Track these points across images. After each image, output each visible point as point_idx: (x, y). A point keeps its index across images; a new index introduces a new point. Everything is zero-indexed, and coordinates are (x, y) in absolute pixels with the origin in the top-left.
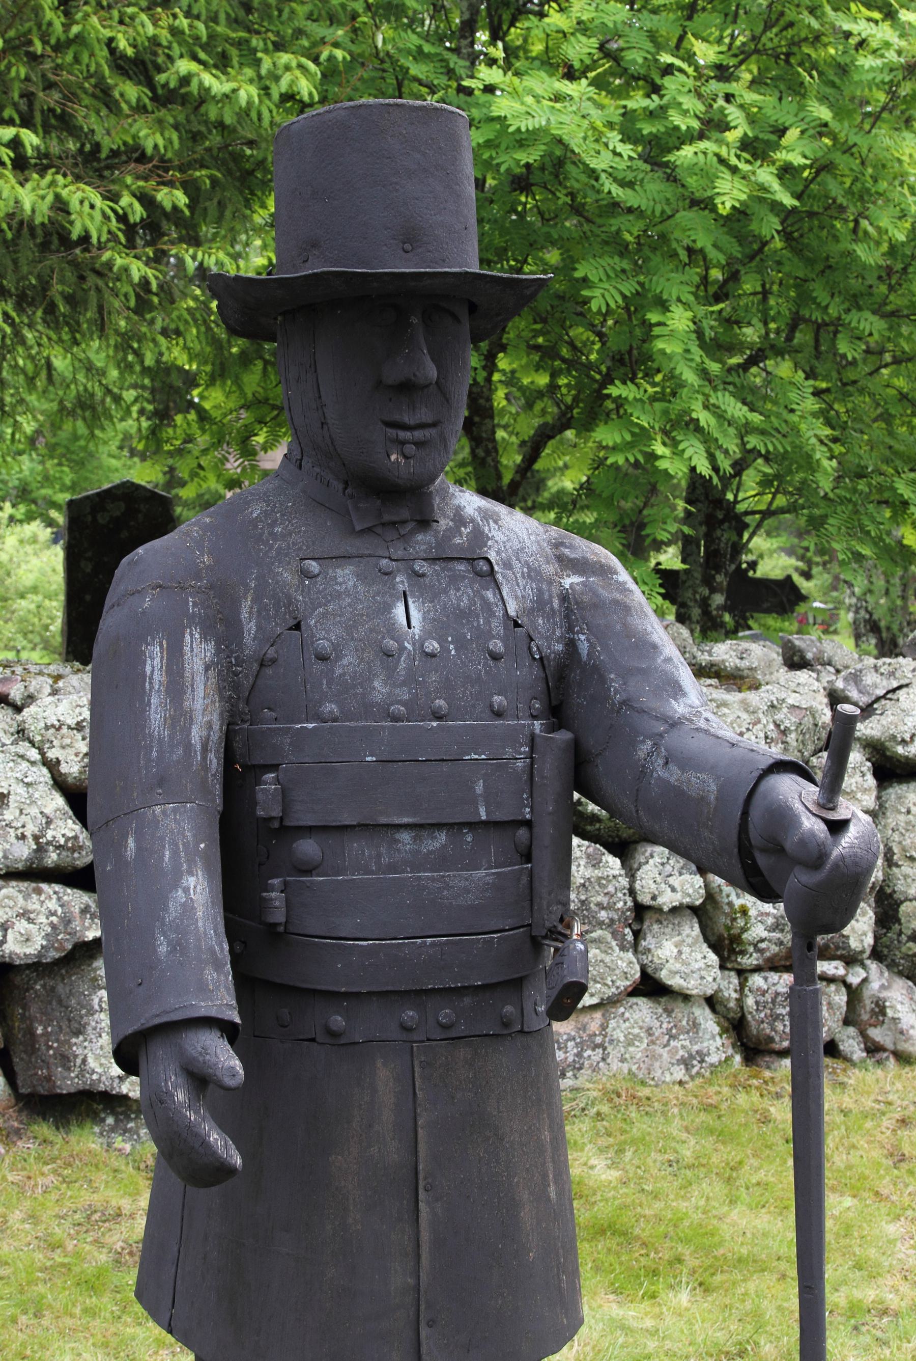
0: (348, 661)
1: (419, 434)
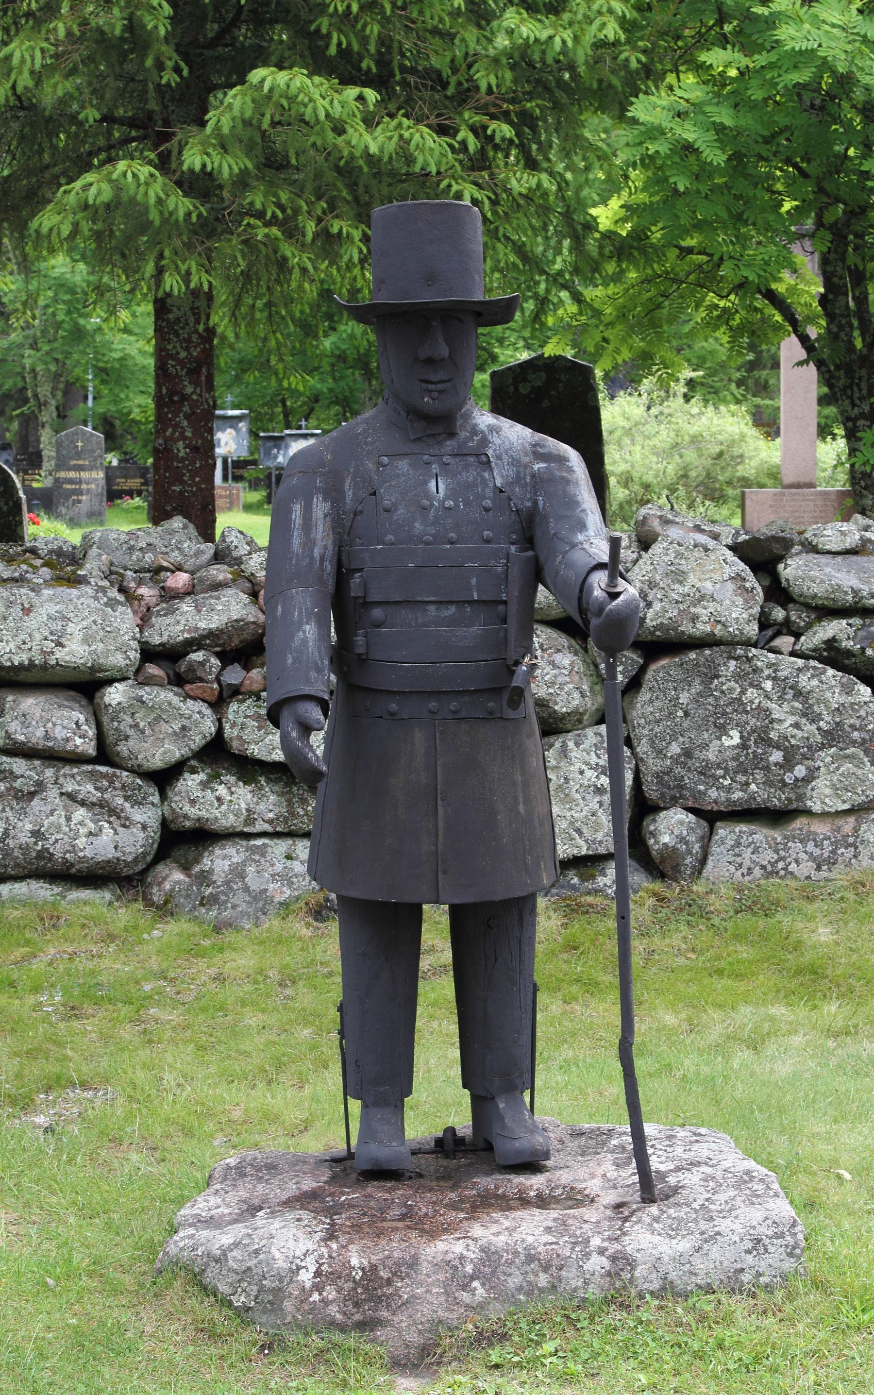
0: (401, 512)
1: (440, 386)
